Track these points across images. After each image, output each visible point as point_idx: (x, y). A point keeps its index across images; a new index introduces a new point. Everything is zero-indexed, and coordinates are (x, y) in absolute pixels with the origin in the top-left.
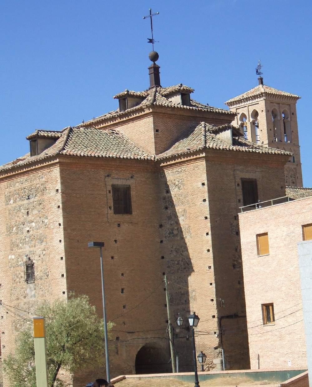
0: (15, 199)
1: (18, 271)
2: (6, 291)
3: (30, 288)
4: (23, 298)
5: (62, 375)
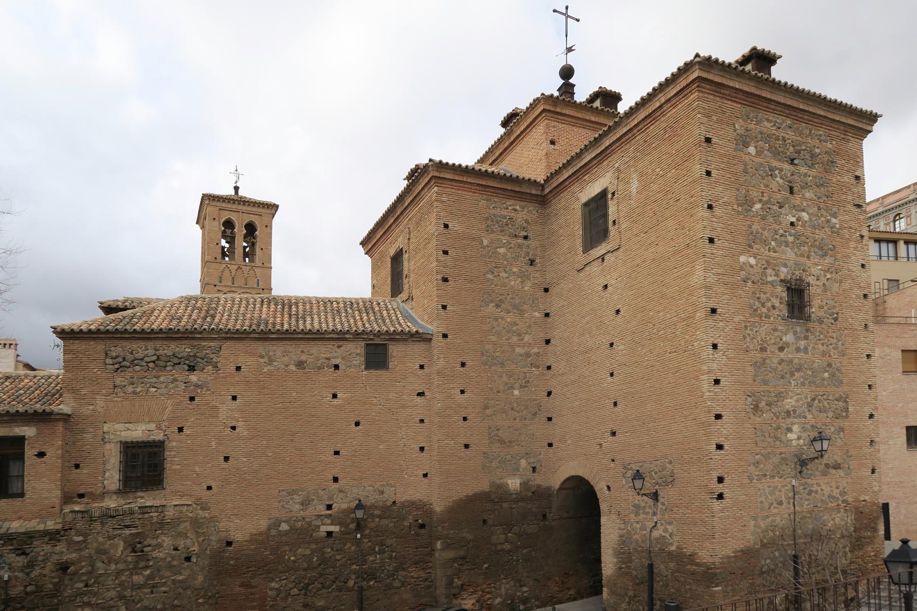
0: (207, 364)
1: (765, 293)
2: (730, 327)
3: (795, 333)
4: (777, 351)
5: (864, 502)
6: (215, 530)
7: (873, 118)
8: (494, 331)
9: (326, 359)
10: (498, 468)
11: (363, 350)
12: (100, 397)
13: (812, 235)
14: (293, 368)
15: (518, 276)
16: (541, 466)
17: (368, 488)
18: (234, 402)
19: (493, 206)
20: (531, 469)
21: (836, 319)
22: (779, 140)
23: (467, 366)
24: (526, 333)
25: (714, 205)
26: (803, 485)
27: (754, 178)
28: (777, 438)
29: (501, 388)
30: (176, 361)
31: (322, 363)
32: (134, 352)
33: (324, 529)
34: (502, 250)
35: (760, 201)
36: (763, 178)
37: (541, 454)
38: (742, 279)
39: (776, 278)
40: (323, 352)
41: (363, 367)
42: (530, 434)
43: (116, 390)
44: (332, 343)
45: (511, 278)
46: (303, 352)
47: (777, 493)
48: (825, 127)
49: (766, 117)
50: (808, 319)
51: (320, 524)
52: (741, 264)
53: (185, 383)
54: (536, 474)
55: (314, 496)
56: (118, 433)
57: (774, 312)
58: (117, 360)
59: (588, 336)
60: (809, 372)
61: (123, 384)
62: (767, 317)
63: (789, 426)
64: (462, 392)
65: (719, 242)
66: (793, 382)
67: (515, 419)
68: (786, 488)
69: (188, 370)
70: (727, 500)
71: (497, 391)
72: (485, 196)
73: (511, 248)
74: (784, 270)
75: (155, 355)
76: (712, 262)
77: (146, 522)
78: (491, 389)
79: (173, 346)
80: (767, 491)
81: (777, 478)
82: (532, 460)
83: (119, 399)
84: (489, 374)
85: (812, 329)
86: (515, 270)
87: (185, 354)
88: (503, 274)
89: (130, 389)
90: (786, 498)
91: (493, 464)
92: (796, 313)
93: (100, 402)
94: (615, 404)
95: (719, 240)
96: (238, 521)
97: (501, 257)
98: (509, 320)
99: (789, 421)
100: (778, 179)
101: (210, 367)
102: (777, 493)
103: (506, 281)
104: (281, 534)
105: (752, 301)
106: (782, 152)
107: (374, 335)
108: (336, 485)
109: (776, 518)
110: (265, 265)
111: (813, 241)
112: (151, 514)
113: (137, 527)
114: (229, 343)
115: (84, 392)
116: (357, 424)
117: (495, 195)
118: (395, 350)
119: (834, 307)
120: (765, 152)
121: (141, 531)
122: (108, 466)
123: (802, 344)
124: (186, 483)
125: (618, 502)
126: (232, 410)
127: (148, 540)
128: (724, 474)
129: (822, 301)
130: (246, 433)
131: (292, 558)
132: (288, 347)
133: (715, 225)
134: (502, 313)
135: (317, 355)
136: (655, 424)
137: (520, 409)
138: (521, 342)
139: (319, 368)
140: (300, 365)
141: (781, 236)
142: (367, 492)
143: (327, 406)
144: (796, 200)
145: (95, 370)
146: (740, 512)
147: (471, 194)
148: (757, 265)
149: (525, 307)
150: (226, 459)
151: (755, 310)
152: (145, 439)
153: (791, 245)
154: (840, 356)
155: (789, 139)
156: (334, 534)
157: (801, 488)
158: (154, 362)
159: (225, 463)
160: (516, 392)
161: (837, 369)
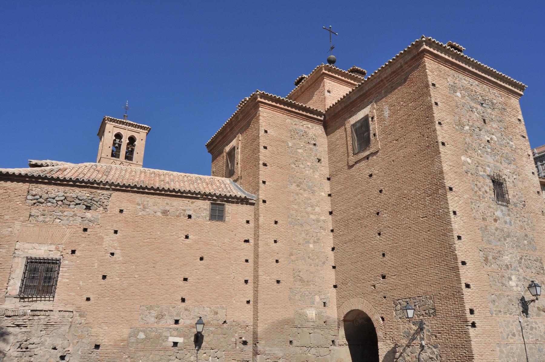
1: (480, 182)
3: (502, 211)
4: (493, 221)
6: (88, 334)
7: (522, 87)
8: (296, 202)
9: (183, 210)
10: (300, 300)
11: (208, 206)
12: (18, 223)
13: (500, 150)
14: (159, 214)
17: (206, 309)
21: (524, 205)
22: (472, 91)
23: (279, 224)
24: (316, 206)
25: (442, 123)
26: (526, 322)
27: (462, 110)
28: (503, 284)
29: (301, 241)
30: (77, 201)
32: (49, 193)
34: (300, 151)
35: (468, 125)
36: (467, 112)
38: (464, 171)
39: (484, 173)
41: (208, 218)
42: (321, 277)
43: (30, 219)
44: (188, 200)
45: (306, 169)
47: (511, 327)
48: (496, 88)
49: (464, 78)
50: (508, 202)
51: (169, 335)
52: (463, 161)
53: (82, 218)
54: (325, 308)
55: (166, 312)
56: (26, 250)
57: (487, 195)
58: (36, 197)
59: (360, 208)
60: (515, 239)
61: (37, 214)
62: (484, 198)
63: (509, 276)
64: (275, 242)
65: (448, 145)
66: (507, 244)
67: (310, 265)
68: (515, 323)
69: (85, 209)
70: (478, 328)
71: (299, 244)
73: (305, 150)
74: (488, 169)
75: (63, 196)
76: (446, 158)
77: (34, 323)
78: (295, 241)
80: (504, 325)
81: (508, 315)
82: (323, 297)
83: (32, 225)
84: (293, 231)
86: (309, 164)
87: (85, 198)
88: (301, 166)
89: (41, 218)
90: (517, 332)
91: (296, 297)
92: (500, 197)
93: (17, 226)
94: (384, 255)
95: (448, 144)
96: (107, 328)
97: (300, 155)
98: (305, 196)
99: (509, 271)
101: (101, 208)
102: (511, 327)
103: (303, 170)
104: (138, 342)
105: (472, 186)
106: (475, 98)
107: (217, 197)
108: (183, 305)
109: (513, 347)
111: (502, 153)
112: (39, 317)
113: (26, 327)
114: (117, 193)
115: (7, 217)
116: (201, 259)
117: (296, 117)
118: (229, 208)
119: (522, 197)
120: (467, 97)
121: (29, 330)
122: (13, 276)
123: (507, 219)
124: (71, 294)
125: (391, 330)
126: (113, 241)
127: (33, 338)
128: (473, 307)
129: (514, 192)
130: (121, 259)
132: (158, 199)
133: (445, 135)
134: (301, 191)
136: (415, 269)
138: (314, 212)
139: (178, 216)
140: (165, 212)
141: (483, 148)
142: (206, 312)
143: (181, 244)
145: (18, 203)
146: (488, 339)
148: (472, 163)
149: (315, 188)
150: (104, 277)
151: (476, 192)
152: (45, 257)
153: (489, 154)
154: (532, 230)
155: (478, 92)
156: (178, 345)
157: (525, 324)
158: (62, 201)
159: (103, 280)
160: (311, 246)
161: (531, 239)
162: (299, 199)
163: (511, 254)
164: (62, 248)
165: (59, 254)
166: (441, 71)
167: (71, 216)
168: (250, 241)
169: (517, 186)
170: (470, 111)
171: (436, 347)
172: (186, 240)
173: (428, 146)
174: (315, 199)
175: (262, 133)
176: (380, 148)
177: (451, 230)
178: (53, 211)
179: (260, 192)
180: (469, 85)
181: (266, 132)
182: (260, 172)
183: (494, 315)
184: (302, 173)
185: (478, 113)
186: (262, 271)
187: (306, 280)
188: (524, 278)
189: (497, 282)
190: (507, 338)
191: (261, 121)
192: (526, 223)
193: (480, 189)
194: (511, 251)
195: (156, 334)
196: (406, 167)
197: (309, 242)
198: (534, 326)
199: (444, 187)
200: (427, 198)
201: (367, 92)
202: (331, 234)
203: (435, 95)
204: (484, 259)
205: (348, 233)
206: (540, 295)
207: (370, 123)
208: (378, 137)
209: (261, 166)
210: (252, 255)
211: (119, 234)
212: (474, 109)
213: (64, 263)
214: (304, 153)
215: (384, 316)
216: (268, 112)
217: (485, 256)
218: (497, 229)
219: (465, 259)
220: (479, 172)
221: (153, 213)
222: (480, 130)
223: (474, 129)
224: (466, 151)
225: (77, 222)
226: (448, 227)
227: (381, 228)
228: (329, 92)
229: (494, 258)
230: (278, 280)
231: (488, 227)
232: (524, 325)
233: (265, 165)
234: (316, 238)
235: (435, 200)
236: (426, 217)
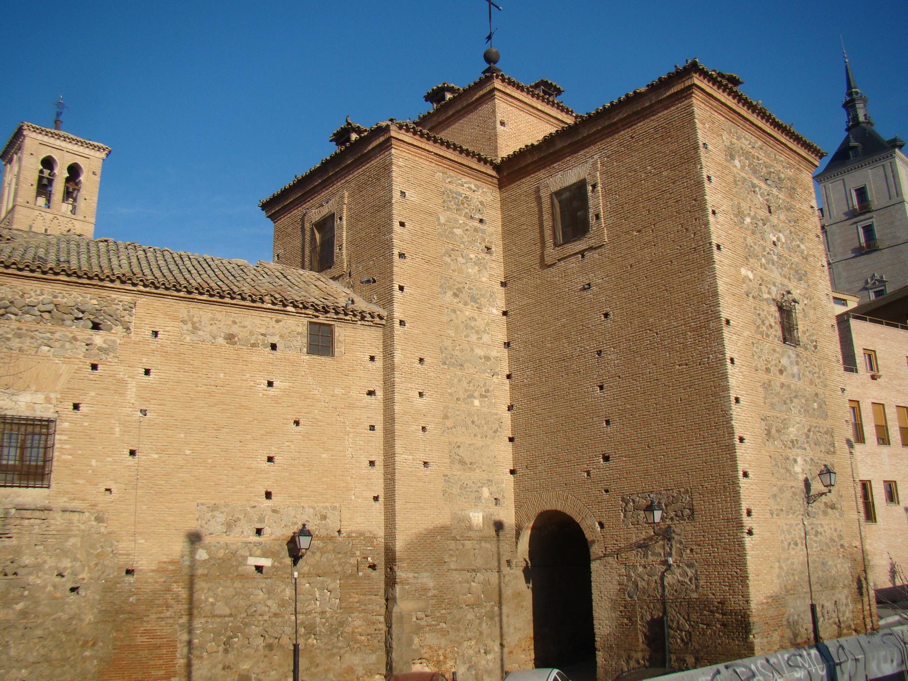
4: (778, 374)
11: (305, 328)
14: (221, 341)
15: (476, 264)
16: (503, 496)
18: (147, 378)
19: (449, 180)
20: (494, 501)
21: (815, 347)
24: (484, 331)
26: (811, 525)
28: (788, 470)
31: (257, 339)
32: (26, 295)
33: (253, 561)
37: (503, 482)
40: (259, 325)
44: (270, 315)
46: (234, 322)
53: (87, 345)
55: (241, 514)
63: (795, 457)
64: (421, 394)
70: (756, 536)
71: (457, 399)
72: (441, 168)
73: (467, 230)
78: (451, 394)
79: (75, 294)
84: (448, 377)
85: (800, 354)
86: (472, 256)
88: (460, 259)
96: (143, 541)
97: (458, 239)
98: (467, 313)
99: (795, 451)
100: (759, 196)
108: (268, 503)
110: (87, 219)
117: (451, 168)
119: (813, 335)
123: (795, 369)
131: (211, 600)
132: (217, 313)
134: (460, 304)
135: (251, 328)
137: (481, 423)
139: (253, 345)
144: (774, 219)
147: (427, 163)
151: (758, 327)
153: (776, 264)
160: (477, 402)
162: (457, 319)
163: (798, 423)
164: (57, 398)
165: (52, 411)
166: (713, 123)
167: (67, 340)
168: (377, 393)
169: (808, 316)
170: (751, 191)
171: (690, 566)
172: (270, 388)
173: (694, 248)
174: (483, 320)
175: (396, 195)
176: (606, 240)
177: (726, 389)
178: (37, 331)
179: (396, 305)
180: (750, 146)
181: (403, 194)
182: (395, 269)
183: (774, 516)
184: (460, 271)
185: (761, 196)
186: (400, 446)
187: (468, 461)
188: (812, 460)
189: (780, 466)
190: (789, 548)
191: (394, 174)
192: (817, 375)
193: (763, 321)
194: (798, 419)
195: (227, 552)
196: (653, 280)
197: (472, 395)
198: (819, 530)
199: (719, 318)
200: (689, 333)
201: (584, 138)
202: (507, 381)
203: (708, 164)
204: (766, 432)
205: (541, 382)
206: (833, 486)
207: (590, 194)
208: (603, 221)
209: (396, 257)
210: (381, 418)
211: (152, 375)
212: (757, 189)
213: (63, 425)
214: (465, 236)
215: (604, 521)
216: (406, 158)
217: (767, 428)
218: (782, 386)
219: (743, 432)
220: (762, 293)
221: (211, 338)
222: (764, 225)
223: (756, 222)
224: (747, 259)
225: (80, 352)
226: (722, 383)
227: (605, 378)
228: (502, 124)
229: (778, 431)
230: (425, 461)
231: (772, 383)
232: (809, 528)
233: (402, 255)
234: (483, 389)
235: (702, 338)
236: (687, 365)
